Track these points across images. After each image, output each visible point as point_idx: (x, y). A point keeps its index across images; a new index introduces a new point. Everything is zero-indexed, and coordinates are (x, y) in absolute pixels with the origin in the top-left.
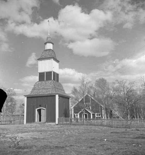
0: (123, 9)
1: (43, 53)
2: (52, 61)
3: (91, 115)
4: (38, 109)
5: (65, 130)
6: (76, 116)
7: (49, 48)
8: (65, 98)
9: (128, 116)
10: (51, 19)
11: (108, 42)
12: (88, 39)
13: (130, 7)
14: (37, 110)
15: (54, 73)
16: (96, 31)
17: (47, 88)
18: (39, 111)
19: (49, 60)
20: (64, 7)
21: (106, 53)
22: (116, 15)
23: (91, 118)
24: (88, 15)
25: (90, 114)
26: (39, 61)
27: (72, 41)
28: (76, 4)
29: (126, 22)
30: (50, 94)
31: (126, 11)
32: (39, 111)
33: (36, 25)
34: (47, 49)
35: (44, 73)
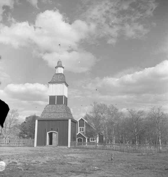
0: (108, 21)
1: (54, 76)
2: (63, 86)
3: (87, 140)
4: (49, 132)
5: (22, 157)
6: (90, 140)
7: (60, 73)
8: (74, 122)
9: (136, 142)
10: (25, 24)
11: (89, 58)
12: (68, 51)
13: (114, 20)
14: (49, 133)
15: (65, 97)
16: (76, 43)
17: (57, 113)
18: (51, 135)
19: (60, 84)
20: (43, 11)
21: (85, 70)
22: (99, 27)
23: (86, 141)
24: (70, 25)
25: (85, 138)
26: (50, 84)
27: (48, 52)
28: (58, 10)
29: (110, 36)
30: (63, 118)
31: (110, 24)
32: (51, 135)
33: (6, 28)
34: (59, 73)
35: (55, 97)
